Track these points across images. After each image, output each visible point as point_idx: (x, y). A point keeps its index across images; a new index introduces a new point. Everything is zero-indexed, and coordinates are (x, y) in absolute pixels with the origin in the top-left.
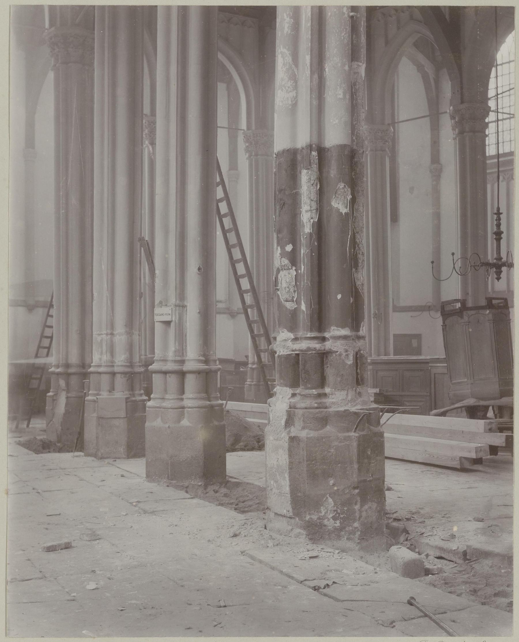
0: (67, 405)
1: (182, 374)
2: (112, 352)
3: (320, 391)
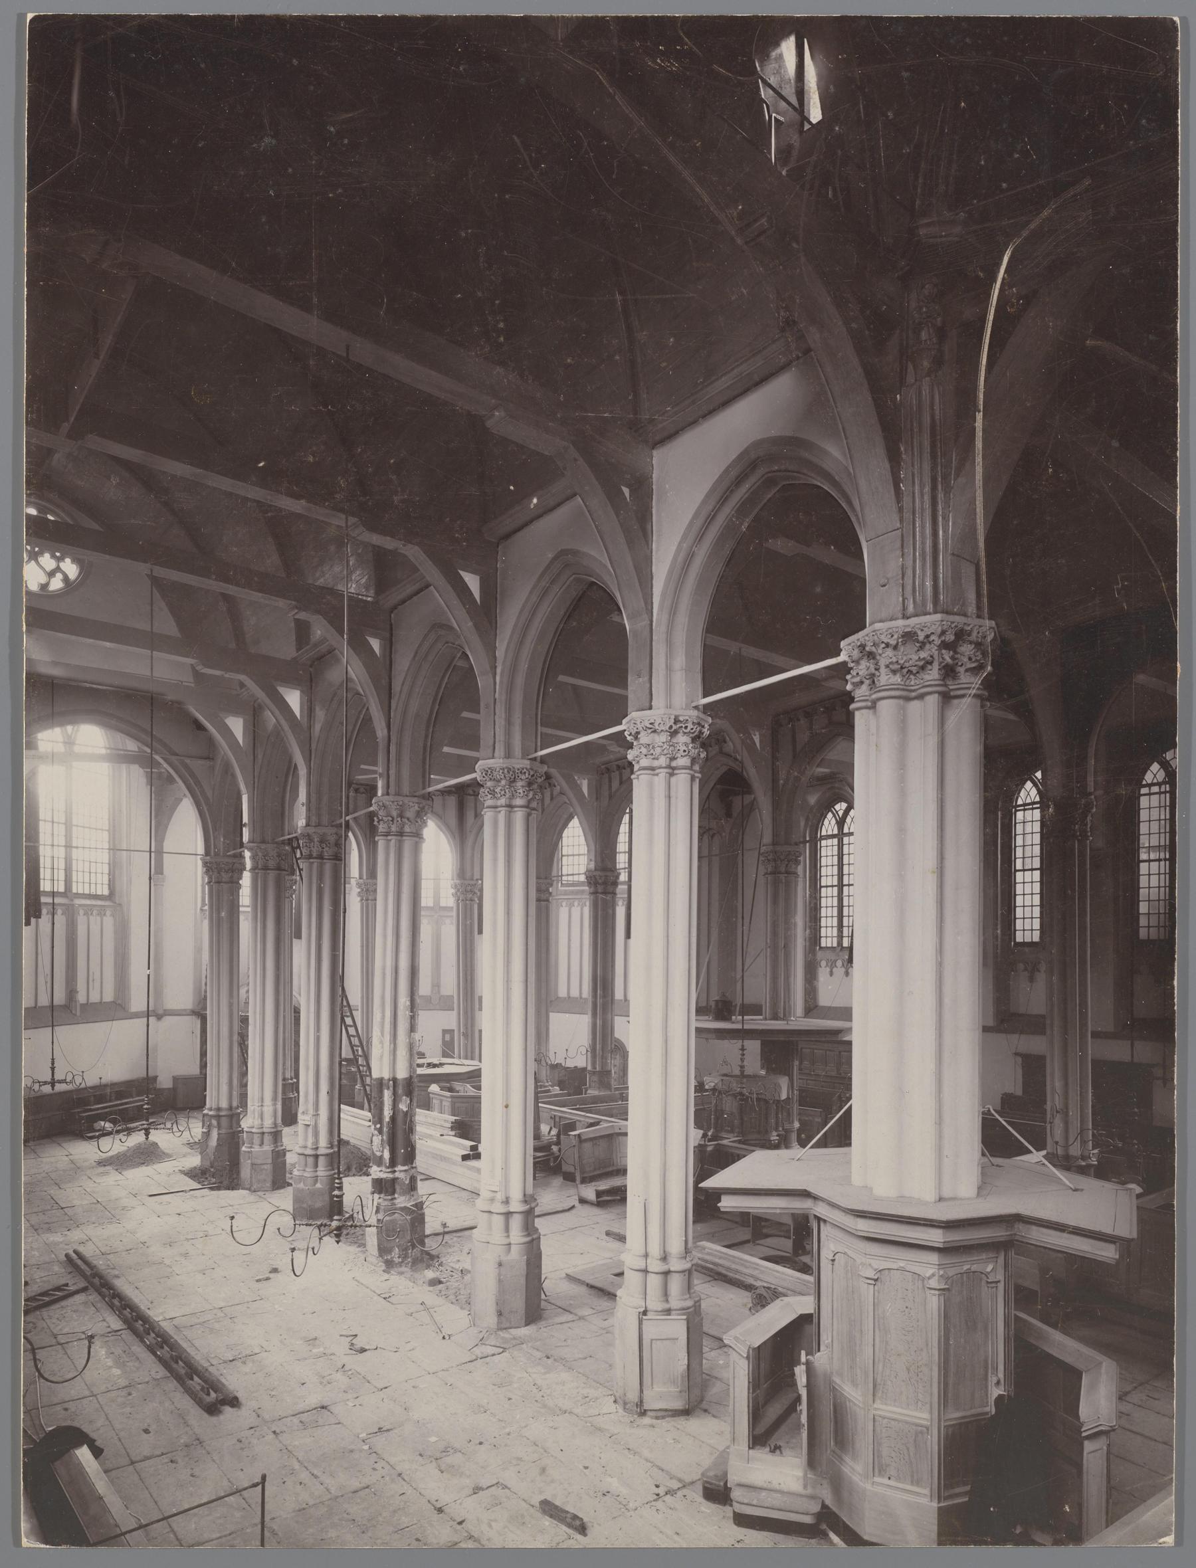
0: (218, 1140)
1: (316, 1156)
2: (262, 1117)
3: (393, 1197)
